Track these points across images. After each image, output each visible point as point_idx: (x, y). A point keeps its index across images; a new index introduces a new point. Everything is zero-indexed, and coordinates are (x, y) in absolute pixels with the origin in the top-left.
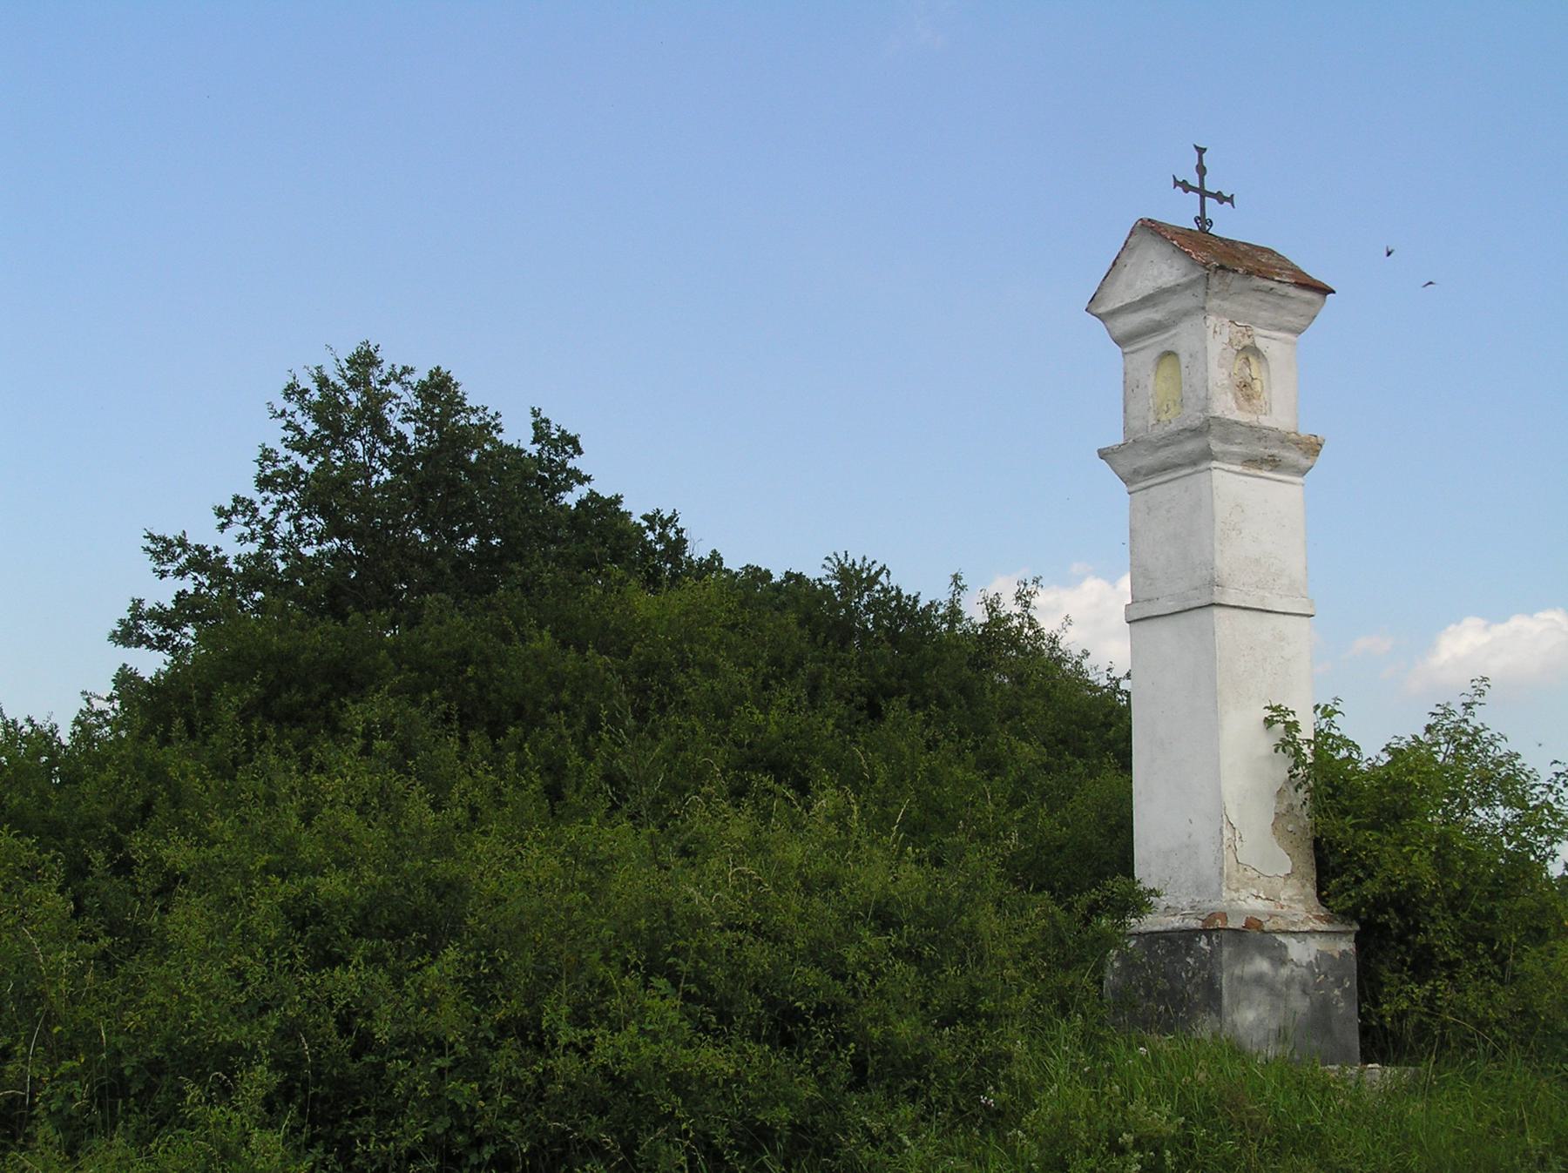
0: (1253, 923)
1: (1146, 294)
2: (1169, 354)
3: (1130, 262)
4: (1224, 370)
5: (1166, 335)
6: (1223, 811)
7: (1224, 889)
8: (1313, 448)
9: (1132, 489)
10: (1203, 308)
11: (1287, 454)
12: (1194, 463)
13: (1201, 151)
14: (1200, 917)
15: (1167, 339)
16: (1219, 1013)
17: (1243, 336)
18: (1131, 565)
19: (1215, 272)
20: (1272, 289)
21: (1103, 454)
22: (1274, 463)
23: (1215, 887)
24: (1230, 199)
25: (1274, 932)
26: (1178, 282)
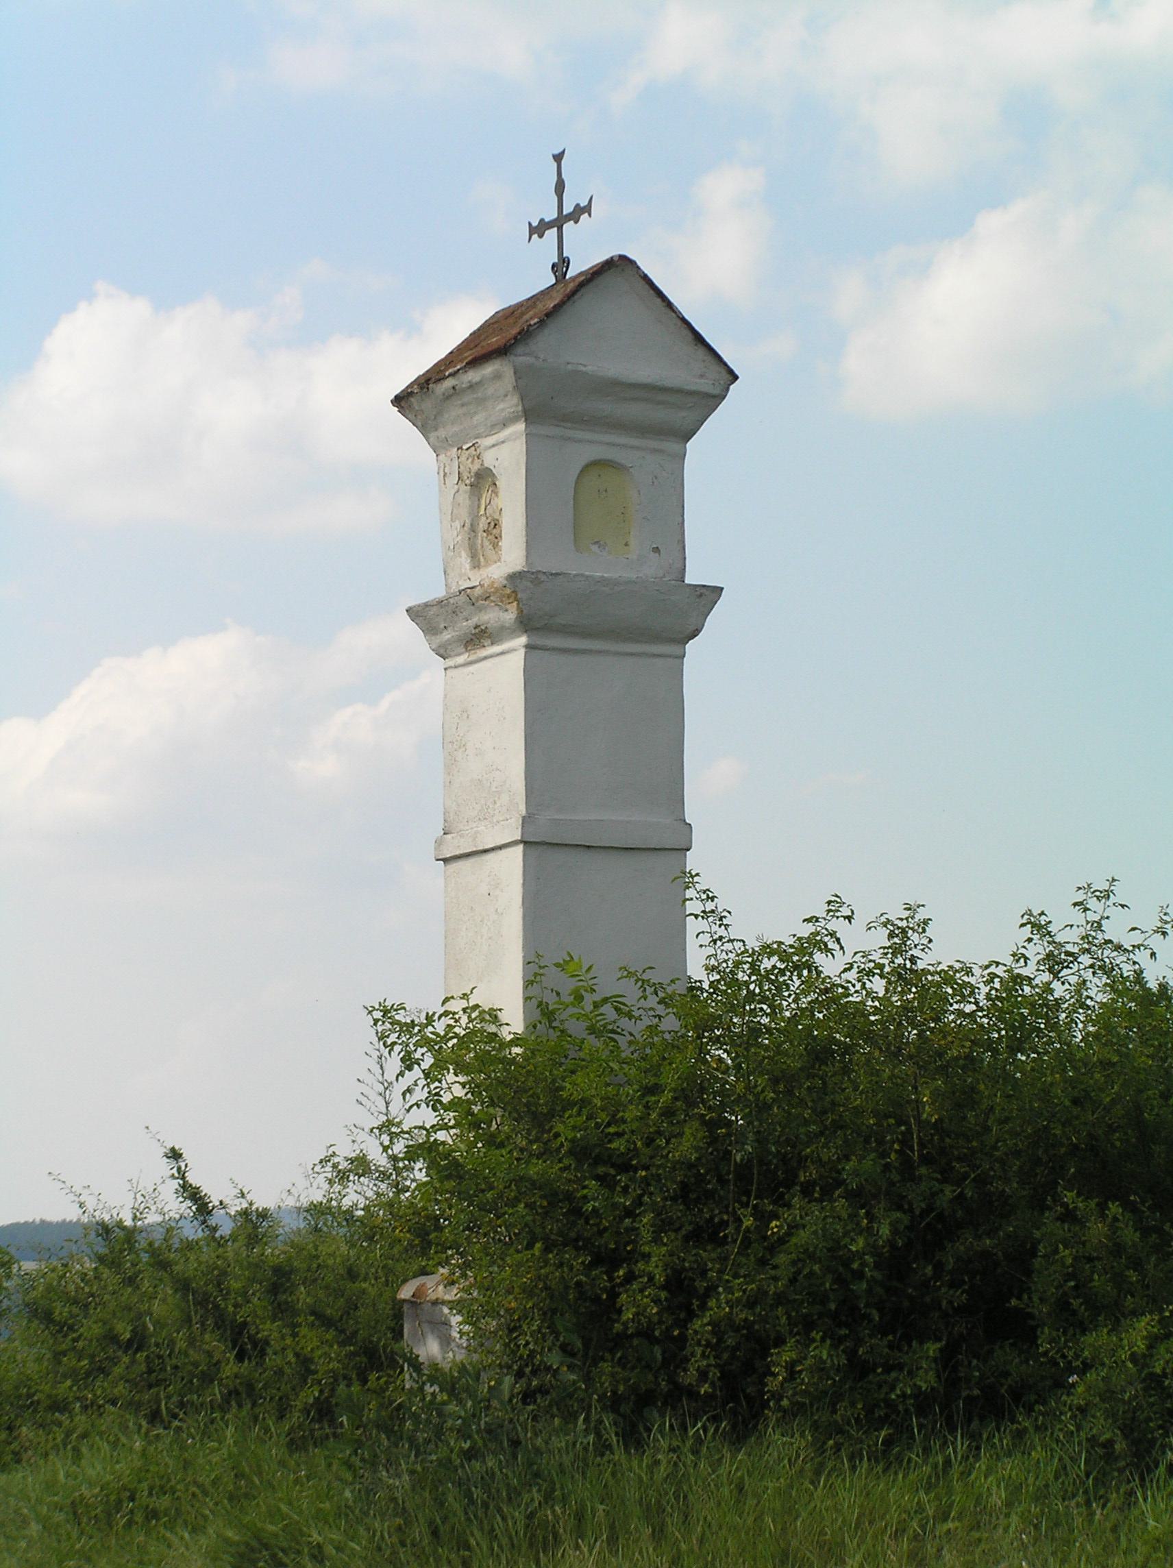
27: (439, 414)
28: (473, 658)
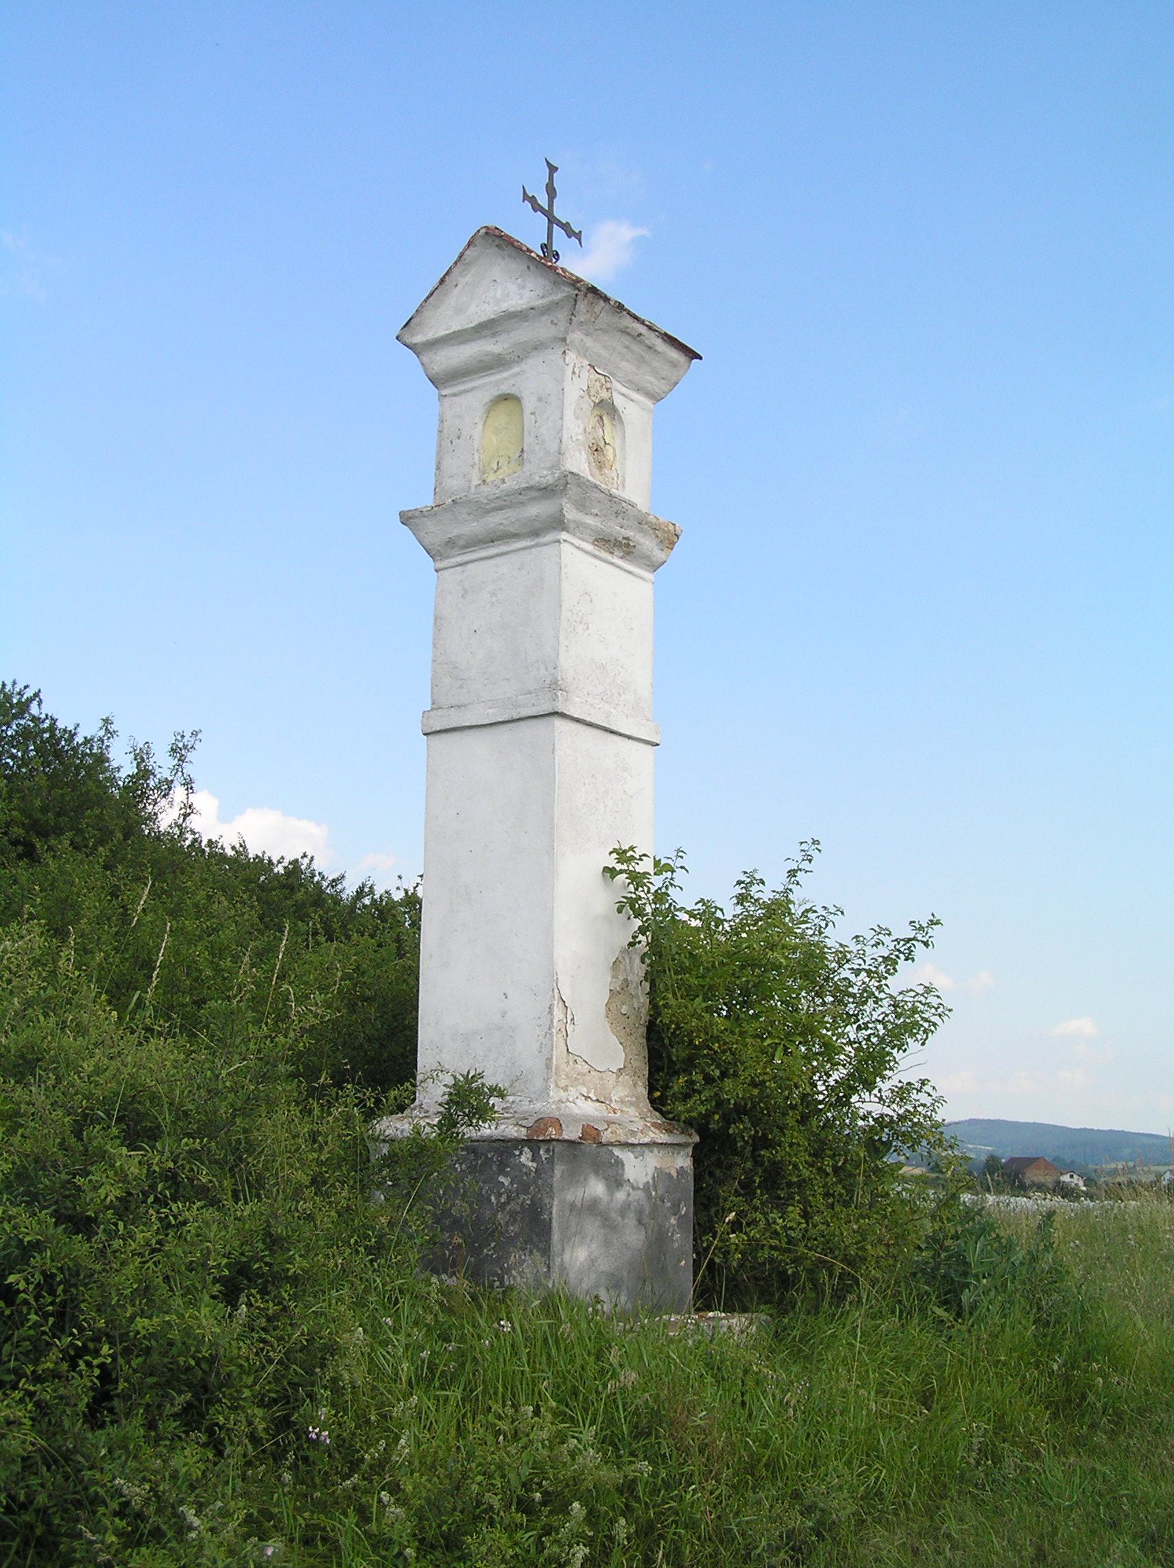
0: (591, 1134)
1: (483, 319)
2: (506, 398)
3: (463, 281)
4: (579, 422)
5: (506, 374)
6: (554, 985)
7: (552, 1086)
8: (669, 539)
9: (441, 565)
10: (564, 340)
11: (642, 540)
12: (535, 533)
13: (552, 169)
14: (524, 1123)
15: (506, 379)
16: (546, 1251)
17: (602, 386)
18: (434, 661)
19: (585, 295)
20: (640, 335)
21: (407, 519)
22: (625, 548)
23: (538, 1084)
24: (578, 236)
25: (612, 1144)
26: (533, 304)
27: (605, 331)
28: (597, 553)
